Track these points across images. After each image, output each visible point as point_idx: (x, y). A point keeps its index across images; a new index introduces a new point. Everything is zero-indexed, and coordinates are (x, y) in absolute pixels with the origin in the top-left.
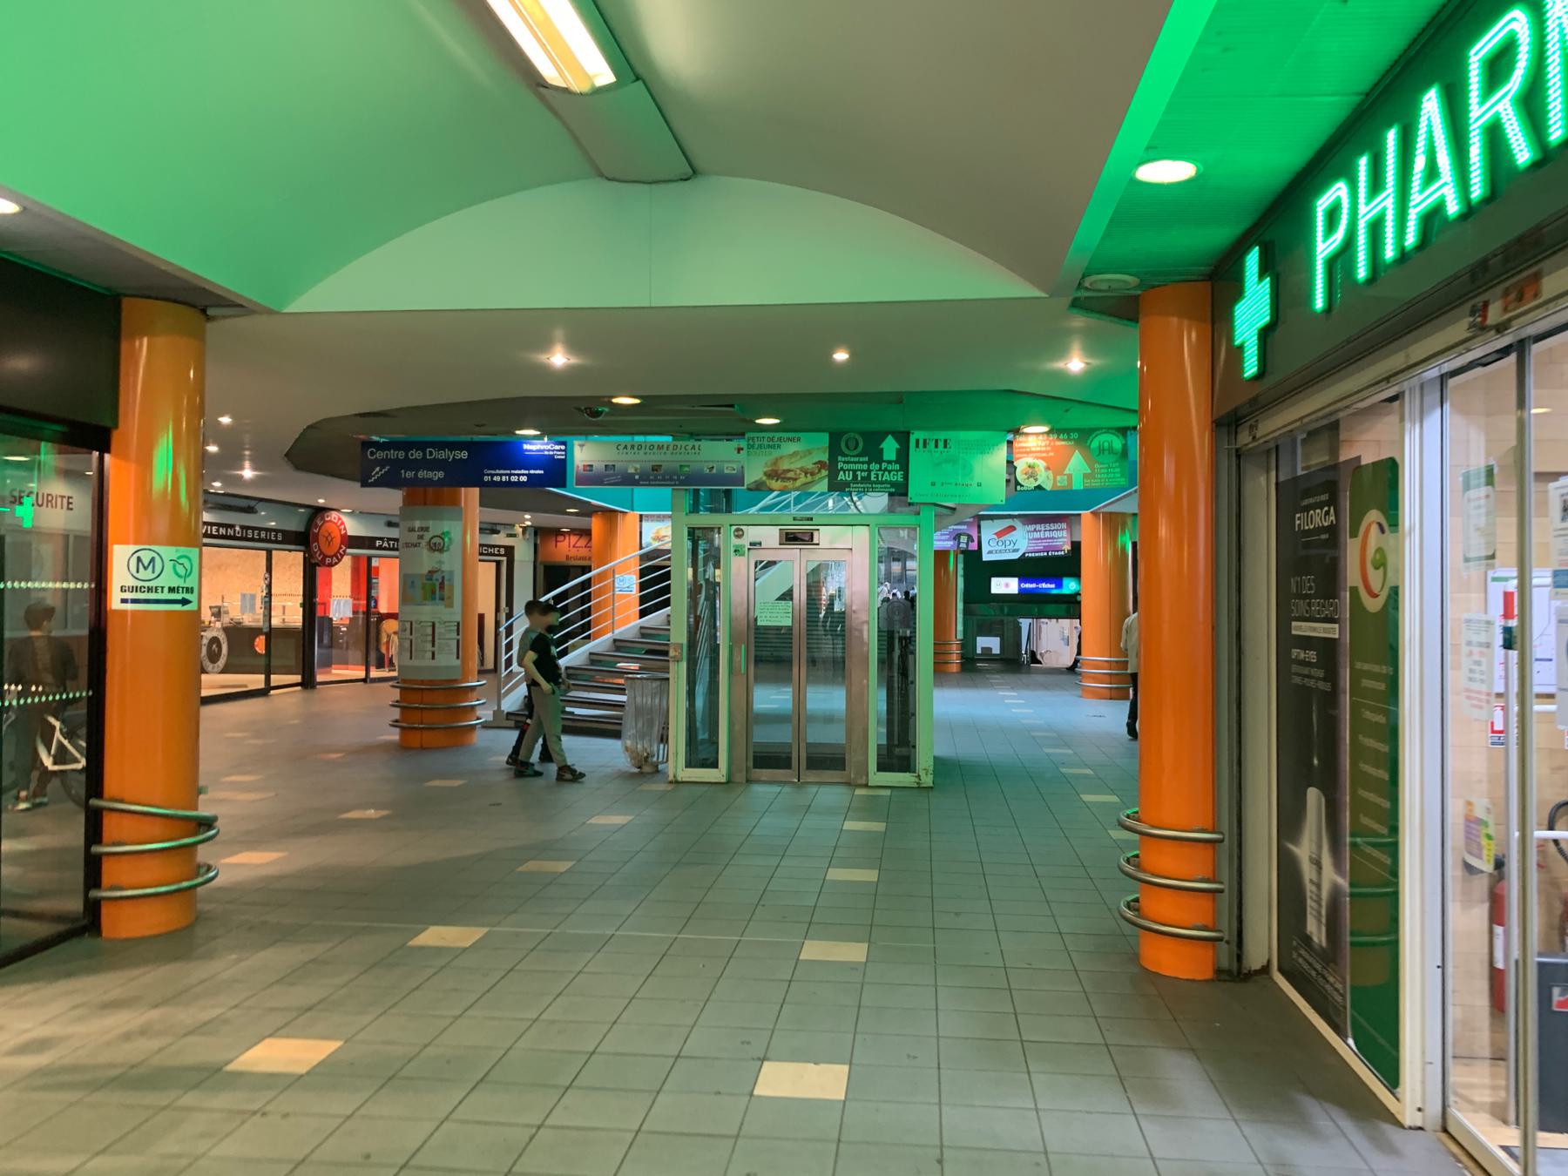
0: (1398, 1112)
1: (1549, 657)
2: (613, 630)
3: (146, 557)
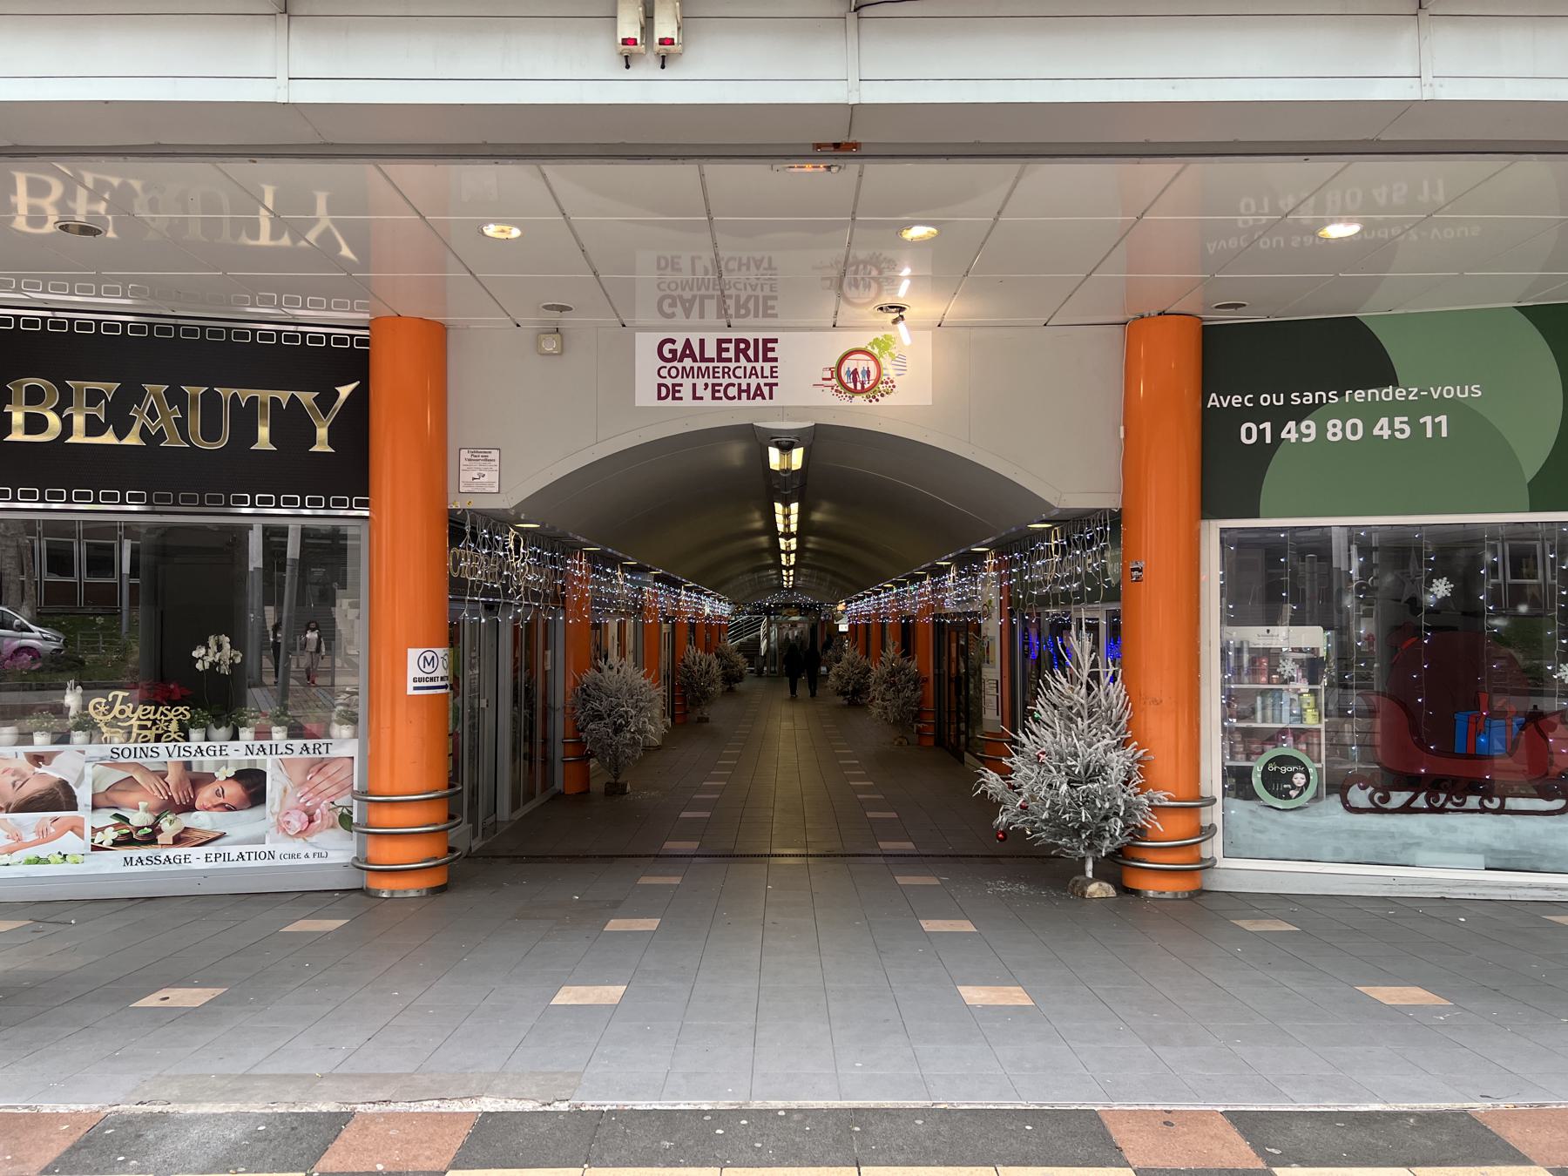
0: (1399, 795)
1: (329, 751)
2: (1346, 745)
3: (429, 656)
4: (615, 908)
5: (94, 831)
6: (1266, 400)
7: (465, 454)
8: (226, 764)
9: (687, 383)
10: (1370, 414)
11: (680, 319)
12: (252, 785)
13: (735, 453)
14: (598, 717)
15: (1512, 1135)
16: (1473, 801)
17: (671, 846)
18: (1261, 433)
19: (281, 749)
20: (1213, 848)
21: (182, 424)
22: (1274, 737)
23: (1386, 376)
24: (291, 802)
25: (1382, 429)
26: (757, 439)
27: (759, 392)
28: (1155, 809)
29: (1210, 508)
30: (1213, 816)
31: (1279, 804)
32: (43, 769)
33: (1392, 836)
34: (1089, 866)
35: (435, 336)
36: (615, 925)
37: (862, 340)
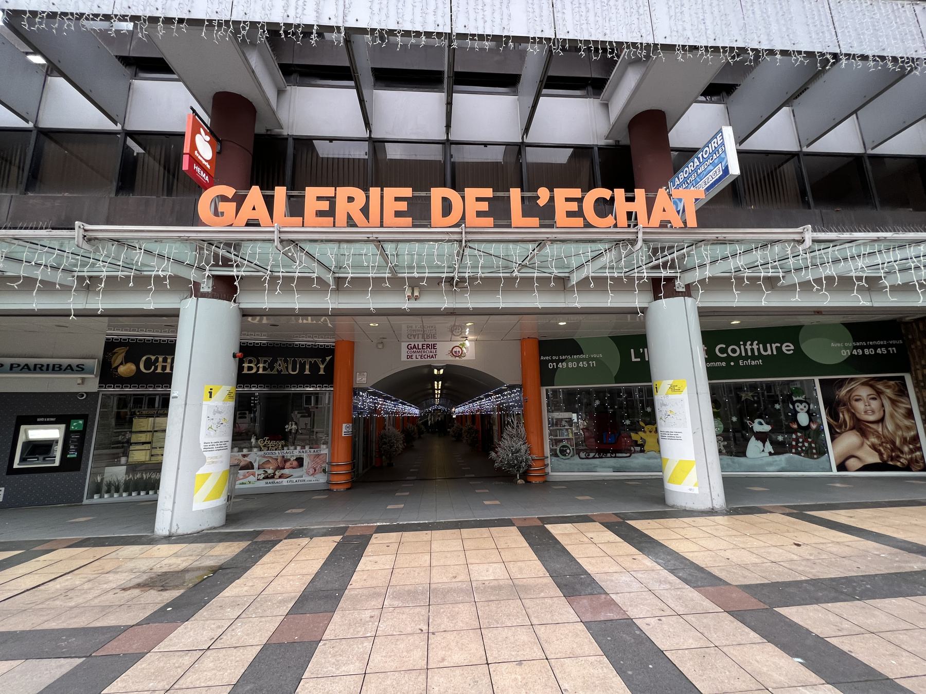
4: (397, 491)
5: (258, 475)
6: (554, 358)
7: (358, 374)
8: (293, 456)
9: (415, 355)
10: (578, 361)
11: (413, 339)
12: (300, 461)
13: (426, 371)
14: (385, 443)
15: (594, 518)
16: (609, 455)
17: (408, 478)
18: (554, 366)
19: (308, 452)
20: (549, 470)
21: (287, 368)
22: (561, 441)
23: (581, 352)
24: (310, 466)
25: (581, 364)
26: (431, 368)
27: (432, 357)
28: (533, 460)
29: (543, 384)
30: (548, 461)
31: (566, 457)
32: (246, 459)
33: (591, 465)
34: (518, 476)
35: (352, 344)
36: (397, 494)
37: (458, 344)
